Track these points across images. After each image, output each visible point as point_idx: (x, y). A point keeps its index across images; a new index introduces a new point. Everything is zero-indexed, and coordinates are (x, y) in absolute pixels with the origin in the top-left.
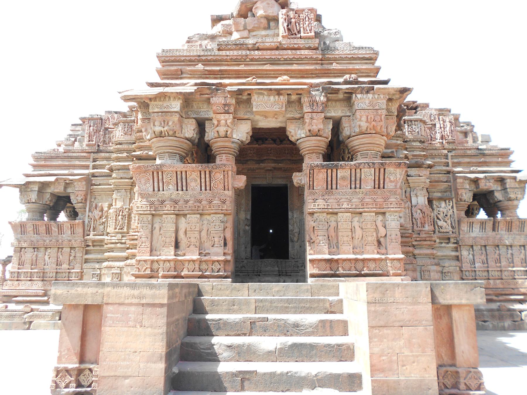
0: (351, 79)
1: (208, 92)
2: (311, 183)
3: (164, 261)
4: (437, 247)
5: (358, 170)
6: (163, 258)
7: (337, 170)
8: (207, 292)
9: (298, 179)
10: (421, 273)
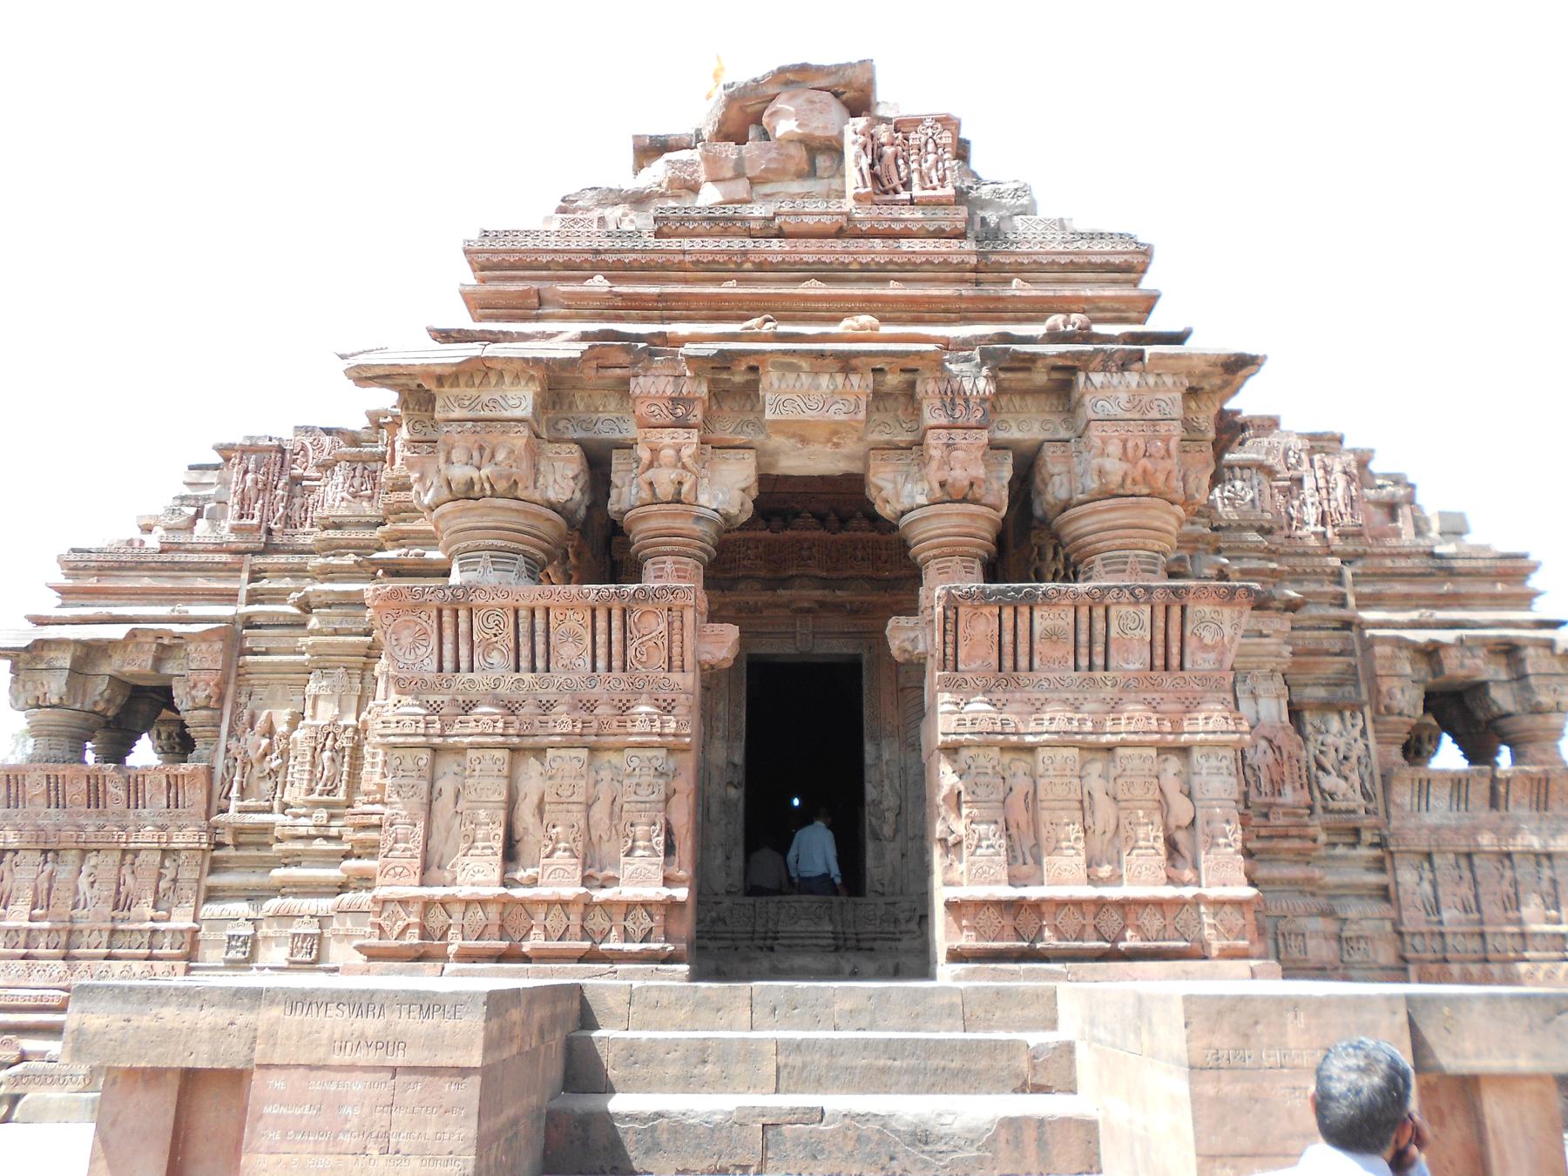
0: (1070, 328)
1: (623, 358)
2: (949, 651)
3: (468, 903)
4: (1320, 858)
5: (1099, 612)
6: (464, 892)
7: (1031, 609)
8: (610, 1013)
9: (901, 635)
10: (1276, 941)
